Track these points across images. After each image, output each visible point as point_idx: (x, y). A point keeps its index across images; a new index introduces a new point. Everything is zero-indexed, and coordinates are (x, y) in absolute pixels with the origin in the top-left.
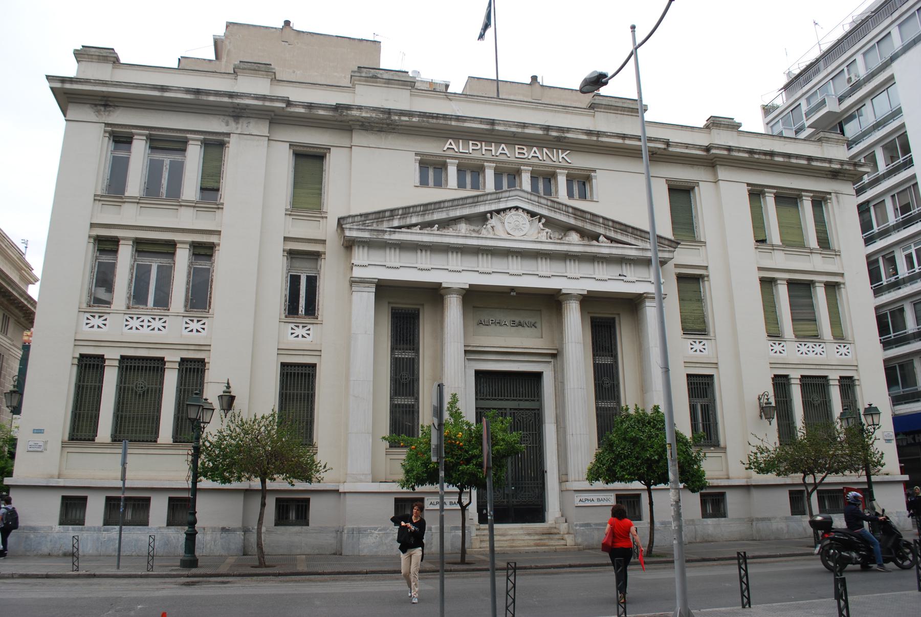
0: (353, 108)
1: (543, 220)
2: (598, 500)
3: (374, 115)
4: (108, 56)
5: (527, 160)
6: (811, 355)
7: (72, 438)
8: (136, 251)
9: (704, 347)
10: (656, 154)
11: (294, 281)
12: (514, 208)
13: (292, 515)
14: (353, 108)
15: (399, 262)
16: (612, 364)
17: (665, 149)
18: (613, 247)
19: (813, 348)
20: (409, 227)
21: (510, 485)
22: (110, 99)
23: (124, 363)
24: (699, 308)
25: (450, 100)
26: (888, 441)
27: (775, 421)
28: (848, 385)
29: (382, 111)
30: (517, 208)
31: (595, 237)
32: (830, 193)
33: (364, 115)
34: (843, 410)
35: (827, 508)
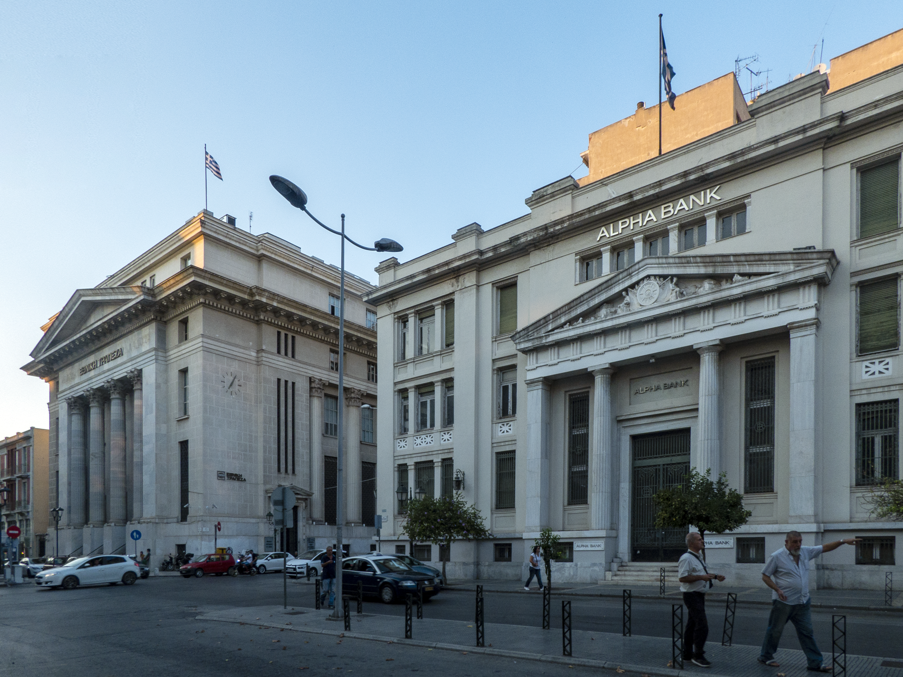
0: (520, 237)
1: (675, 280)
2: (592, 546)
3: (535, 236)
4: (475, 230)
5: (674, 217)
7: (858, 484)
8: (419, 394)
11: (505, 389)
12: (646, 277)
13: (877, 554)
14: (520, 237)
15: (656, 336)
17: (838, 127)
18: (745, 284)
20: (562, 326)
21: (661, 530)
23: (860, 410)
25: (606, 185)
29: (541, 229)
30: (648, 277)
31: (729, 277)
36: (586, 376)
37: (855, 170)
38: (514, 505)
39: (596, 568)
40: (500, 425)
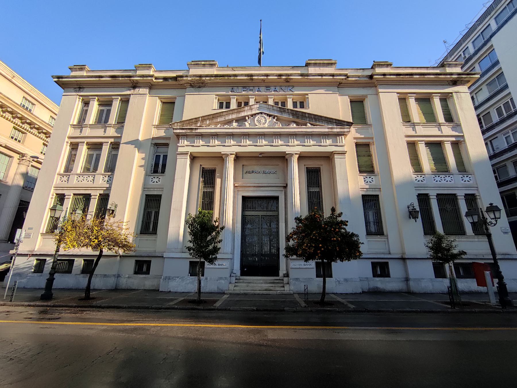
1: (276, 118)
6: (443, 182)
9: (451, 179)
10: (342, 83)
11: (158, 157)
16: (319, 191)
19: (444, 178)
22: (81, 85)
24: (369, 160)
26: (506, 233)
27: (419, 219)
28: (471, 199)
32: (452, 93)
33: (189, 79)
34: (468, 210)
35: (462, 274)
36: (221, 158)
37: (83, 103)
38: (156, 232)
39: (223, 282)
40: (152, 177)
